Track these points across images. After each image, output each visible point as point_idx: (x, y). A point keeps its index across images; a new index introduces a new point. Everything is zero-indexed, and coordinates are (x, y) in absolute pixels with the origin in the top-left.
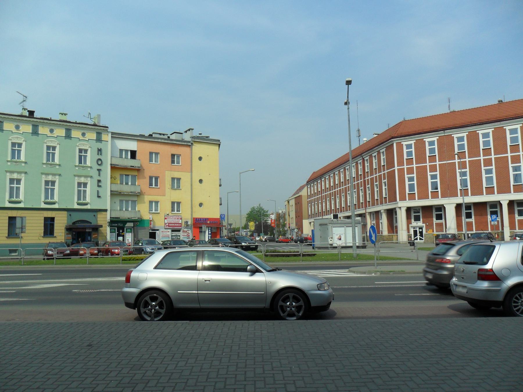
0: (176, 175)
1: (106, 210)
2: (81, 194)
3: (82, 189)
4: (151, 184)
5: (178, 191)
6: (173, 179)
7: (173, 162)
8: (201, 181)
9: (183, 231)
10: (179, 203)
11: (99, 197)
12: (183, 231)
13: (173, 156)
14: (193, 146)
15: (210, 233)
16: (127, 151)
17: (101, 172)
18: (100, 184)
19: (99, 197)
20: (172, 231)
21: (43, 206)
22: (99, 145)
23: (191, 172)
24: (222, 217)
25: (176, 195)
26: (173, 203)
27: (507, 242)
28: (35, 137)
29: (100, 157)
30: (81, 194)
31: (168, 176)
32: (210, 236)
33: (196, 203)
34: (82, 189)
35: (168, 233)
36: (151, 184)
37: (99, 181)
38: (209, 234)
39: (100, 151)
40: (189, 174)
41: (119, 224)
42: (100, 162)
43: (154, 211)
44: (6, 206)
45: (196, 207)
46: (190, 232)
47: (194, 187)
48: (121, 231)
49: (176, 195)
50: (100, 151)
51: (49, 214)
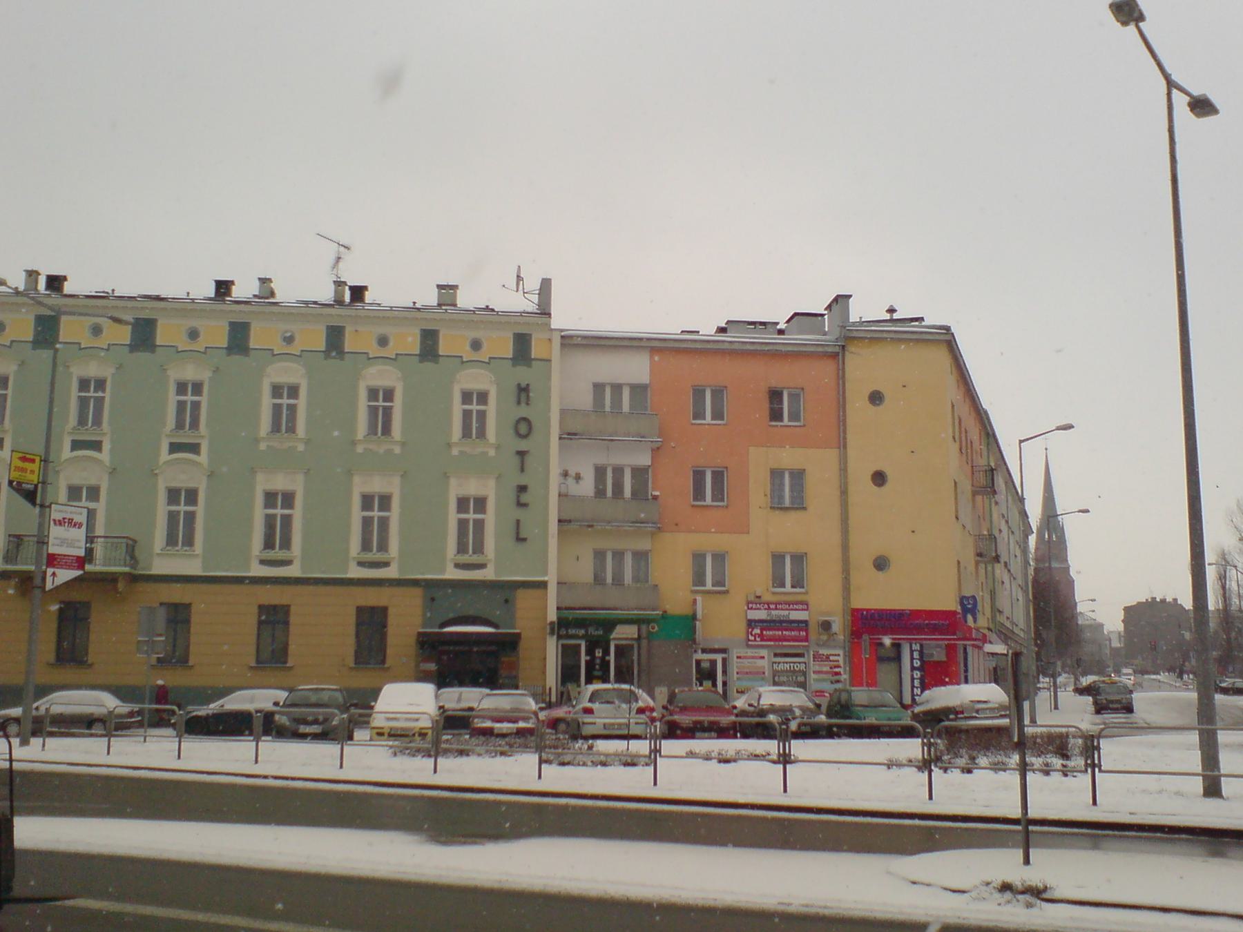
0: (788, 457)
1: (543, 585)
2: (470, 537)
3: (376, 514)
4: (699, 493)
5: (793, 515)
6: (776, 474)
7: (776, 415)
8: (879, 478)
9: (817, 657)
10: (799, 559)
11: (520, 539)
12: (817, 657)
13: (775, 395)
14: (848, 356)
15: (917, 663)
16: (617, 388)
17: (529, 460)
18: (525, 498)
19: (520, 539)
20: (776, 655)
21: (355, 572)
22: (523, 375)
23: (842, 445)
24: (969, 605)
25: (787, 531)
26: (778, 559)
27: (417, 666)
28: (429, 365)
29: (523, 411)
30: (470, 537)
31: (759, 461)
32: (917, 674)
33: (862, 556)
34: (376, 514)
35: (760, 663)
36: (699, 493)
37: (522, 489)
38: (913, 668)
39: (523, 391)
40: (832, 455)
41: (591, 631)
42: (524, 427)
43: (709, 586)
44: (447, 576)
45: (864, 574)
46: (841, 659)
47: (853, 498)
48: (599, 653)
49: (787, 531)
50: (523, 391)
51: (371, 598)
